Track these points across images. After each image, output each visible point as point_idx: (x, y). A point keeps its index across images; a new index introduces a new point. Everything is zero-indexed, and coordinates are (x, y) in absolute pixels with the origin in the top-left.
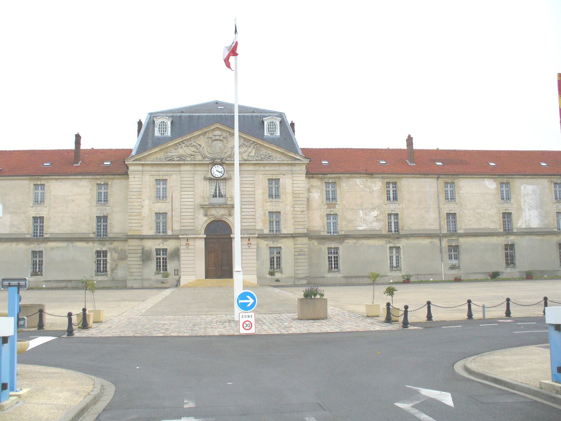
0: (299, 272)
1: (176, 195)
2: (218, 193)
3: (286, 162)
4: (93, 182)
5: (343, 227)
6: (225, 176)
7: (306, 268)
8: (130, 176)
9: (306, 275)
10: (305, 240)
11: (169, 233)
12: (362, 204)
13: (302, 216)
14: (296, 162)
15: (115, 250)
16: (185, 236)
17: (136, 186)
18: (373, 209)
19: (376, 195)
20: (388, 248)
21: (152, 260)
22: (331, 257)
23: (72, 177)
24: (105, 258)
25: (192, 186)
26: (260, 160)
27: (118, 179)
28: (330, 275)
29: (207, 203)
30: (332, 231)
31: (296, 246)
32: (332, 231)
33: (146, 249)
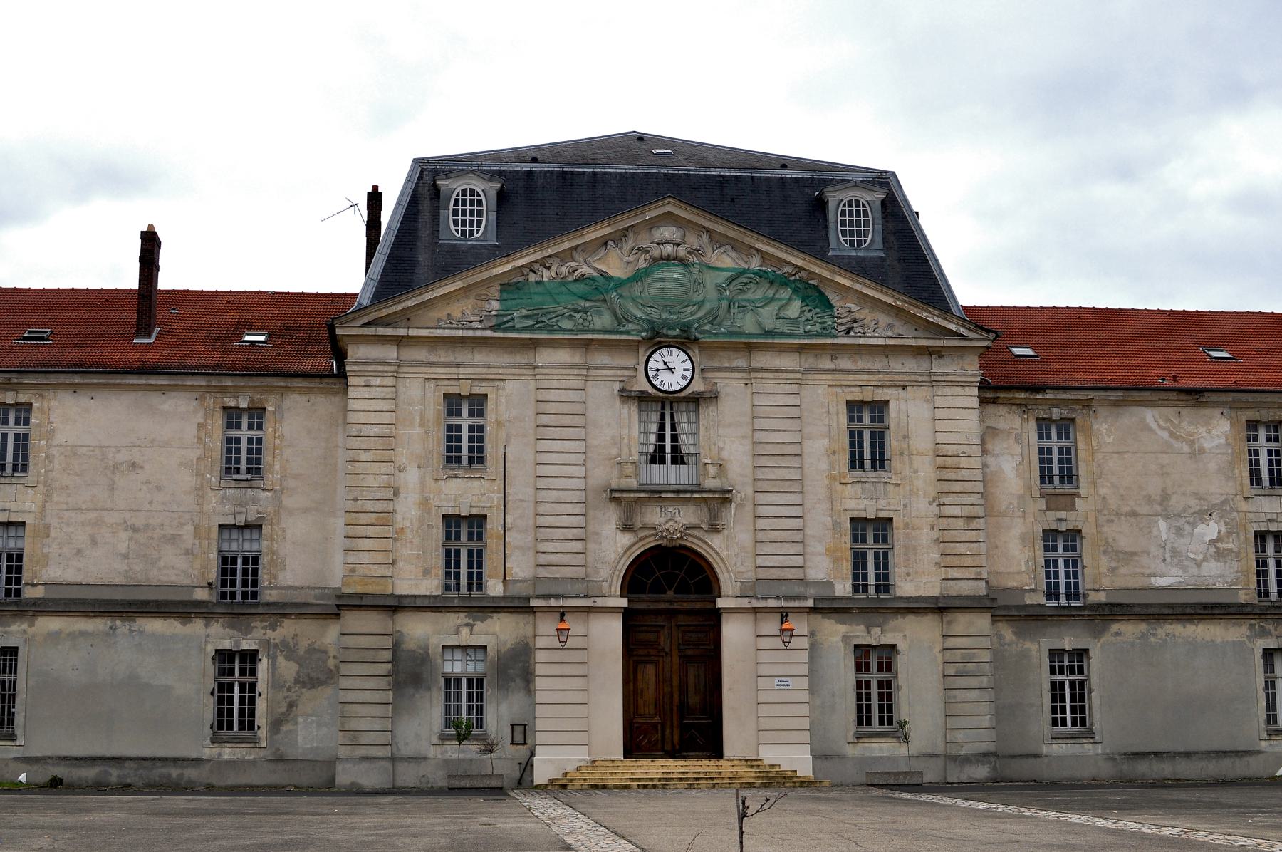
0: (960, 736)
1: (521, 454)
2: (668, 449)
3: (912, 342)
4: (209, 401)
5: (1101, 578)
6: (698, 386)
7: (986, 721)
8: (351, 381)
9: (983, 747)
10: (982, 622)
11: (494, 588)
12: (1165, 497)
13: (971, 535)
14: (947, 343)
15: (288, 649)
16: (553, 602)
17: (374, 418)
18: (1205, 515)
19: (1212, 466)
20: (1259, 653)
21: (429, 689)
22: (1062, 684)
23: (133, 380)
24: (247, 680)
25: (578, 420)
26: (818, 335)
27: (302, 391)
28: (1058, 749)
29: (633, 483)
30: (1062, 590)
31: (951, 642)
32: (1062, 590)
33: (409, 645)
